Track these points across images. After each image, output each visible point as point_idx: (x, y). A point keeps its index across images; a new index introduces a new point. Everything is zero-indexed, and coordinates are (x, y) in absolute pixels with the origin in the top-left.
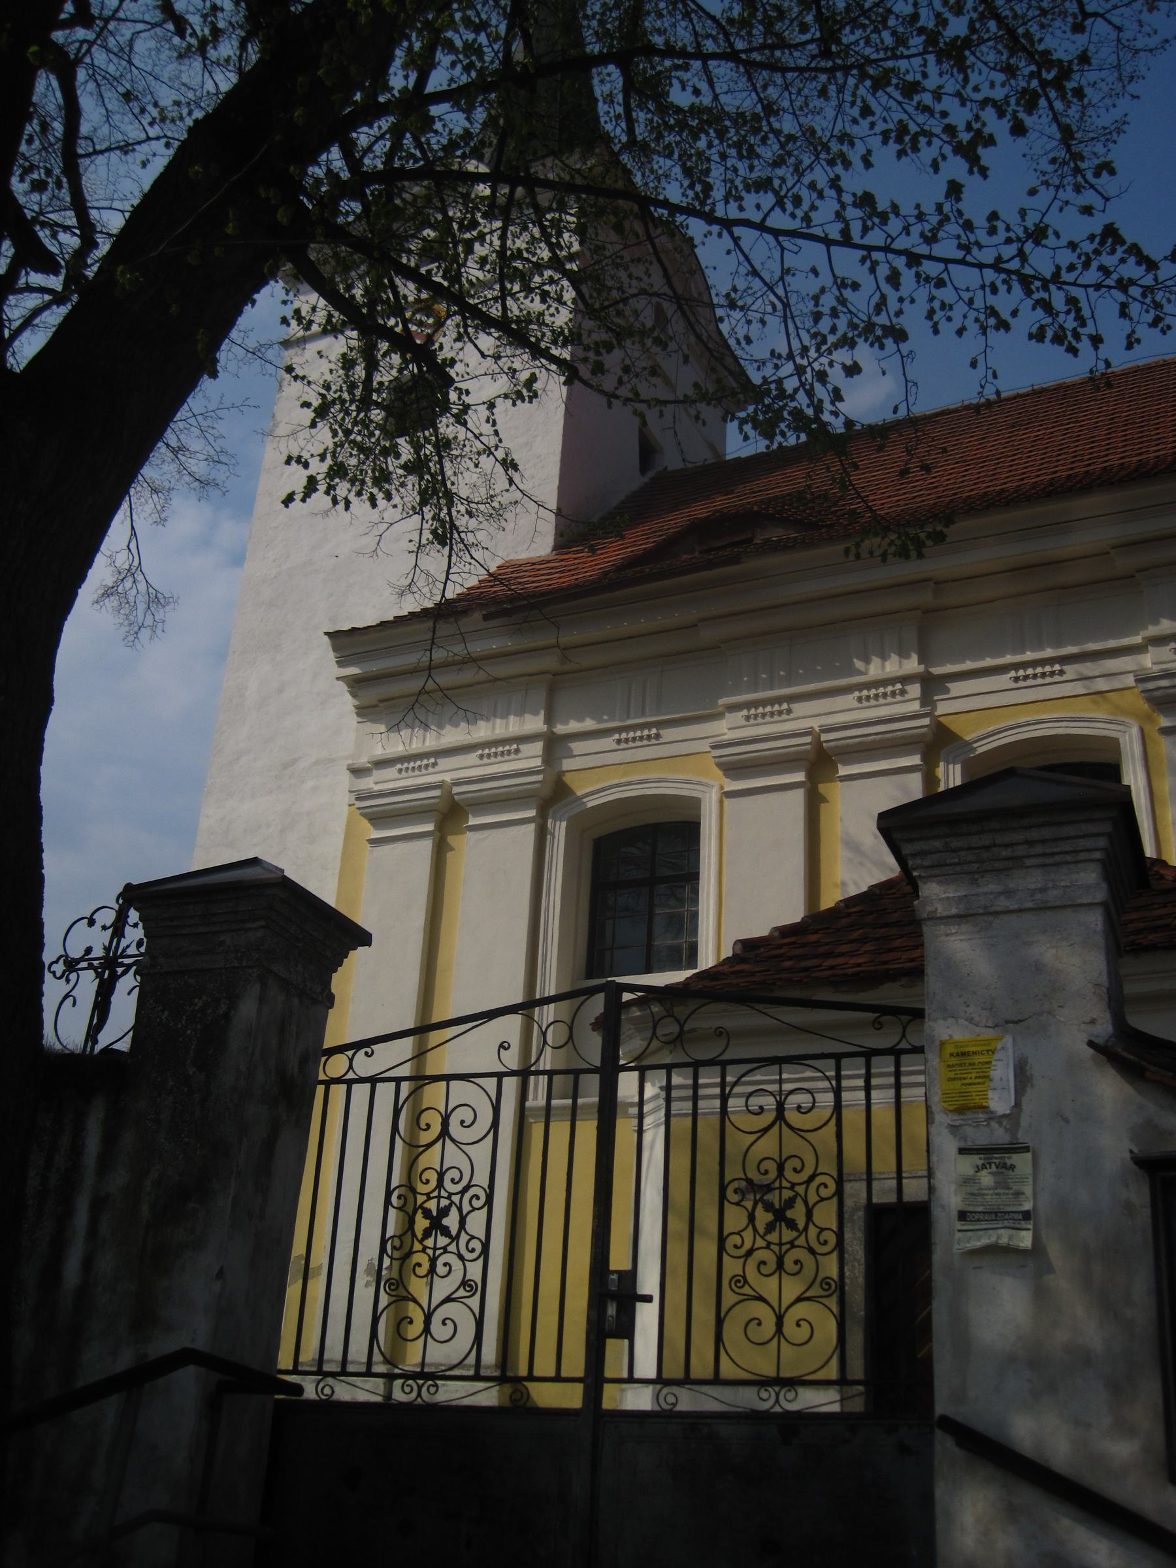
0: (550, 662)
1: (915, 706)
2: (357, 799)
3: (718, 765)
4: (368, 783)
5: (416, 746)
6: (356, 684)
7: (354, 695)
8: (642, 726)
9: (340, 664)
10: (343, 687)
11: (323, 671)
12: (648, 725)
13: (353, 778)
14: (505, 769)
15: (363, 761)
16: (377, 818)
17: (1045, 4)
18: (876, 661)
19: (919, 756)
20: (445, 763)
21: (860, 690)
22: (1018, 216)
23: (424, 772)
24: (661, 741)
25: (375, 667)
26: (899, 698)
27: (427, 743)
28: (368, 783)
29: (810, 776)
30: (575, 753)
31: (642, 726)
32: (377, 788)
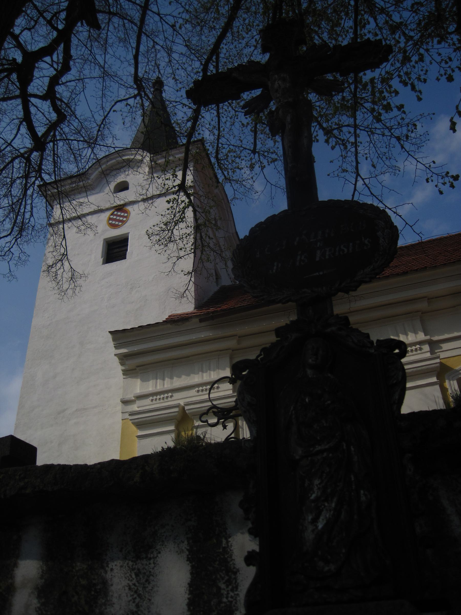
0: (232, 343)
1: (428, 355)
2: (130, 415)
3: (133, 423)
4: (135, 407)
5: (159, 388)
6: (123, 358)
7: (122, 364)
9: (116, 347)
10: (116, 359)
11: (110, 352)
14: (216, 396)
15: (130, 396)
16: (140, 425)
17: (3, 193)
18: (167, 380)
19: (435, 378)
20: (177, 395)
22: (373, 168)
23: (166, 400)
25: (135, 348)
26: (419, 352)
27: (166, 386)
28: (135, 407)
29: (177, 427)
32: (137, 409)
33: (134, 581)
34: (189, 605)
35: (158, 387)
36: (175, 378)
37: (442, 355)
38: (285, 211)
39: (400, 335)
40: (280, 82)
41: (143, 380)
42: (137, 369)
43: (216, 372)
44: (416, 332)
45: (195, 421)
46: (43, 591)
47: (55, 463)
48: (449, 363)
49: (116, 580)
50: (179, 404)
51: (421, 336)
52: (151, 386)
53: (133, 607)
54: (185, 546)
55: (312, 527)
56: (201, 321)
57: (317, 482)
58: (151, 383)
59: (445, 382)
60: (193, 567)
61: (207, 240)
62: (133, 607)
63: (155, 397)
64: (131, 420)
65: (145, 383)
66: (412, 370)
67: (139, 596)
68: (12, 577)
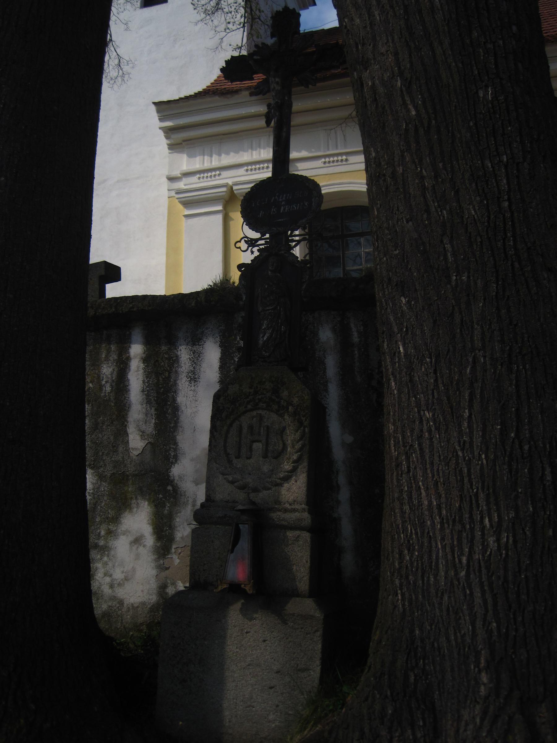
2: (176, 193)
3: (180, 202)
5: (207, 165)
6: (168, 132)
7: (167, 138)
8: (337, 155)
9: (161, 120)
10: (161, 134)
12: (341, 154)
13: (170, 183)
16: (187, 204)
20: (225, 174)
21: (247, 166)
23: (213, 178)
24: (348, 162)
27: (213, 163)
29: (225, 207)
30: (299, 169)
31: (337, 155)
33: (192, 356)
34: (219, 368)
35: (206, 165)
36: (223, 155)
38: (270, 178)
40: (275, 85)
41: (190, 156)
42: (183, 143)
46: (145, 360)
47: (148, 294)
49: (183, 355)
50: (227, 183)
52: (197, 163)
53: (192, 369)
54: (218, 339)
55: (263, 338)
56: (251, 94)
57: (266, 322)
58: (198, 159)
60: (222, 350)
61: (257, 12)
62: (192, 369)
63: (202, 175)
64: (177, 198)
65: (192, 159)
67: (195, 363)
68: (129, 353)
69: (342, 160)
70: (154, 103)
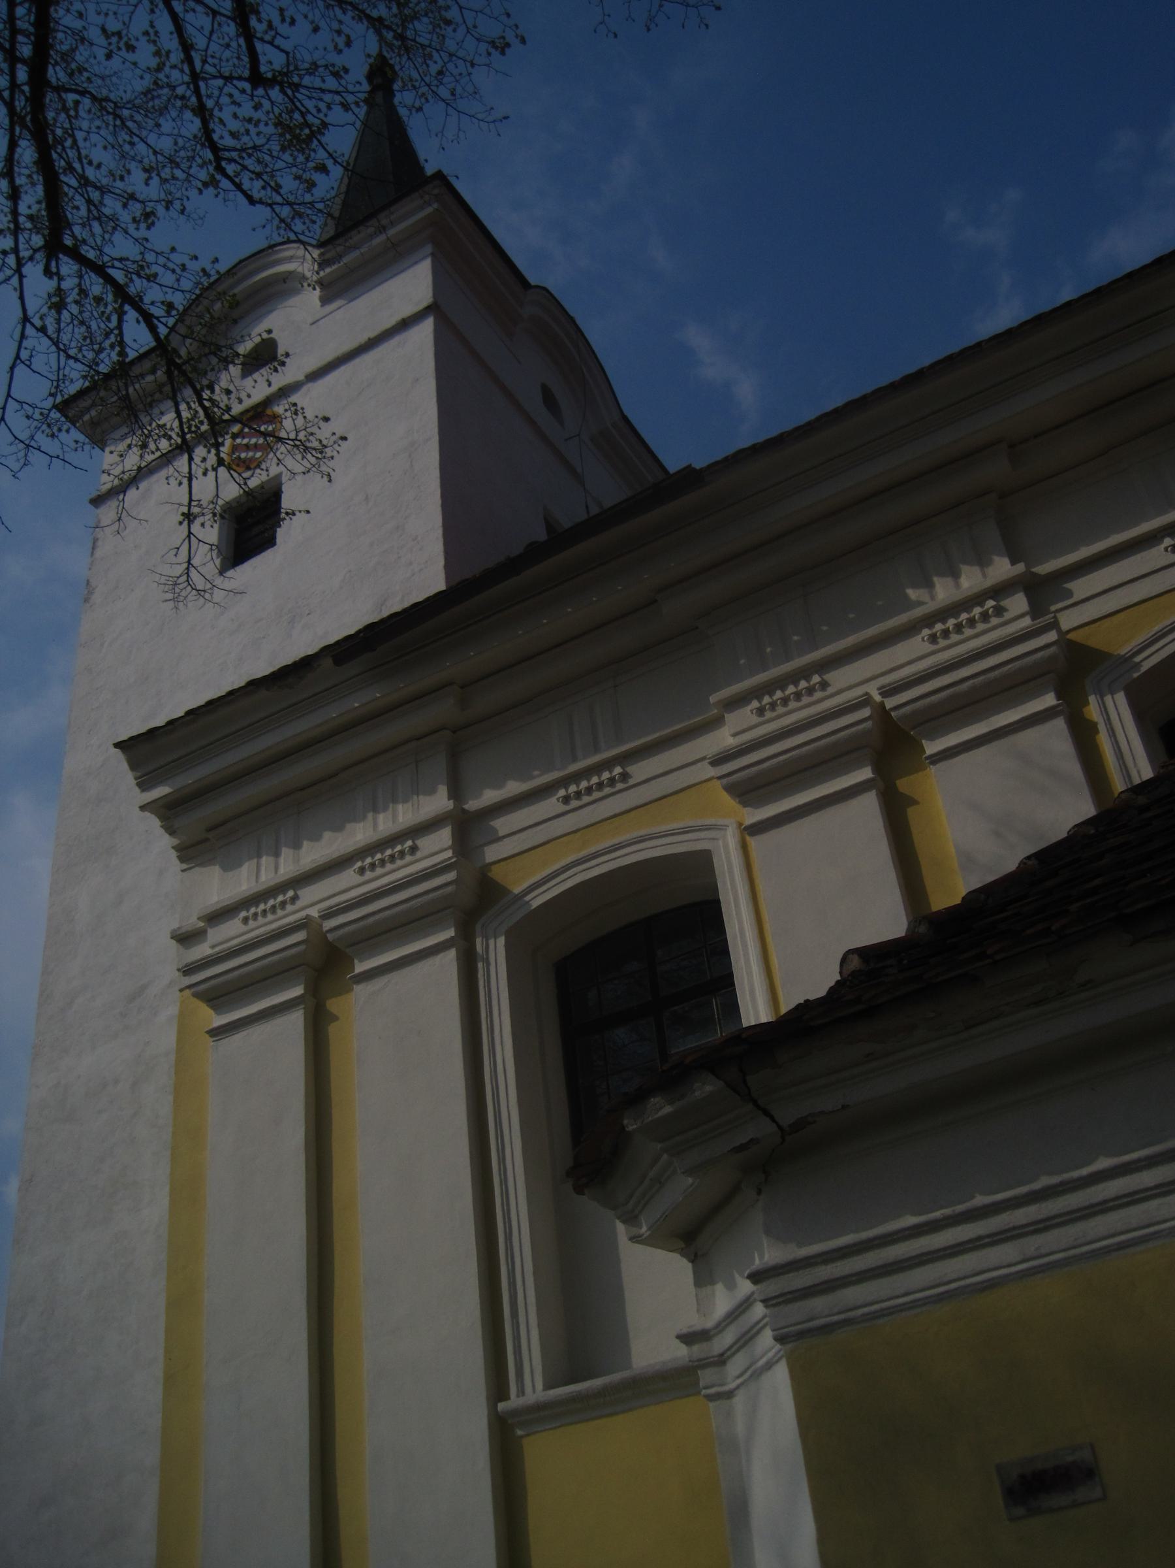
1: (1027, 621)
5: (267, 878)
6: (169, 812)
7: (171, 831)
8: (597, 769)
9: (144, 784)
12: (608, 764)
15: (193, 922)
18: (286, 852)
24: (631, 782)
25: (188, 779)
26: (995, 621)
29: (877, 770)
30: (501, 834)
31: (597, 769)
32: (209, 951)
37: (1068, 620)
39: (935, 579)
41: (226, 868)
43: (410, 804)
44: (982, 561)
45: (356, 961)
48: (1095, 639)
50: (307, 916)
51: (1002, 568)
52: (245, 879)
59: (1087, 703)
65: (231, 874)
66: (971, 682)
69: (612, 781)
70: (118, 745)
